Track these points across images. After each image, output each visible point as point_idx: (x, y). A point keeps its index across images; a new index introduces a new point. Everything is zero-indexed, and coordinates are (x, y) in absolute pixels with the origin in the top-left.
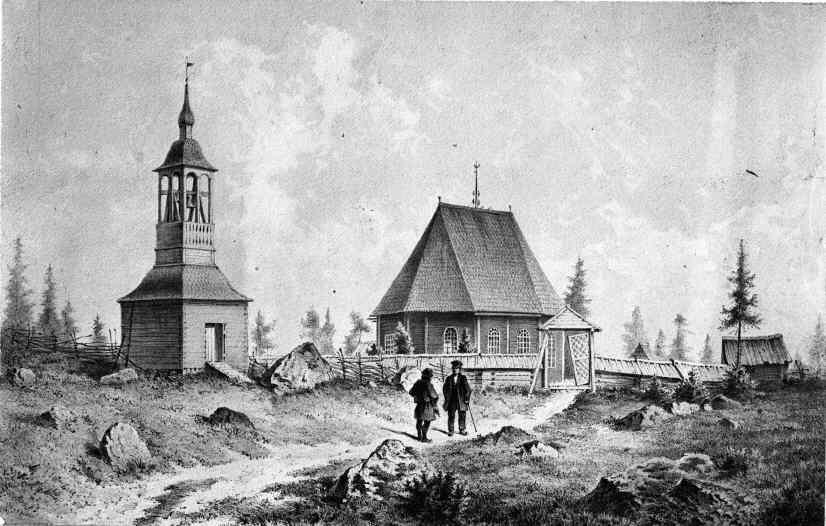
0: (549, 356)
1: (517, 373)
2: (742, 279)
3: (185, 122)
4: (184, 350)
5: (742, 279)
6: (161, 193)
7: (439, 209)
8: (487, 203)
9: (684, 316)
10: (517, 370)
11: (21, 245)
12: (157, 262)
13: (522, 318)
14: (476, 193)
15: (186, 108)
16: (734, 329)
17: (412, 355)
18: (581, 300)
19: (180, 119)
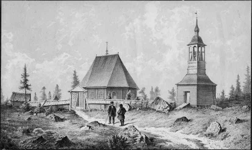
0: (84, 101)
1: (96, 105)
2: (25, 75)
3: (197, 31)
4: (196, 96)
5: (25, 75)
6: (204, 52)
7: (115, 56)
8: (111, 53)
9: (46, 87)
10: (93, 104)
11: (247, 71)
12: (216, 87)
13: (92, 88)
14: (107, 51)
15: (197, 26)
16: (24, 90)
17: (126, 100)
18: (74, 82)
19: (179, 118)
